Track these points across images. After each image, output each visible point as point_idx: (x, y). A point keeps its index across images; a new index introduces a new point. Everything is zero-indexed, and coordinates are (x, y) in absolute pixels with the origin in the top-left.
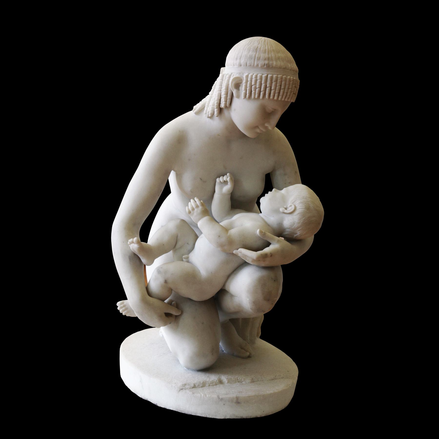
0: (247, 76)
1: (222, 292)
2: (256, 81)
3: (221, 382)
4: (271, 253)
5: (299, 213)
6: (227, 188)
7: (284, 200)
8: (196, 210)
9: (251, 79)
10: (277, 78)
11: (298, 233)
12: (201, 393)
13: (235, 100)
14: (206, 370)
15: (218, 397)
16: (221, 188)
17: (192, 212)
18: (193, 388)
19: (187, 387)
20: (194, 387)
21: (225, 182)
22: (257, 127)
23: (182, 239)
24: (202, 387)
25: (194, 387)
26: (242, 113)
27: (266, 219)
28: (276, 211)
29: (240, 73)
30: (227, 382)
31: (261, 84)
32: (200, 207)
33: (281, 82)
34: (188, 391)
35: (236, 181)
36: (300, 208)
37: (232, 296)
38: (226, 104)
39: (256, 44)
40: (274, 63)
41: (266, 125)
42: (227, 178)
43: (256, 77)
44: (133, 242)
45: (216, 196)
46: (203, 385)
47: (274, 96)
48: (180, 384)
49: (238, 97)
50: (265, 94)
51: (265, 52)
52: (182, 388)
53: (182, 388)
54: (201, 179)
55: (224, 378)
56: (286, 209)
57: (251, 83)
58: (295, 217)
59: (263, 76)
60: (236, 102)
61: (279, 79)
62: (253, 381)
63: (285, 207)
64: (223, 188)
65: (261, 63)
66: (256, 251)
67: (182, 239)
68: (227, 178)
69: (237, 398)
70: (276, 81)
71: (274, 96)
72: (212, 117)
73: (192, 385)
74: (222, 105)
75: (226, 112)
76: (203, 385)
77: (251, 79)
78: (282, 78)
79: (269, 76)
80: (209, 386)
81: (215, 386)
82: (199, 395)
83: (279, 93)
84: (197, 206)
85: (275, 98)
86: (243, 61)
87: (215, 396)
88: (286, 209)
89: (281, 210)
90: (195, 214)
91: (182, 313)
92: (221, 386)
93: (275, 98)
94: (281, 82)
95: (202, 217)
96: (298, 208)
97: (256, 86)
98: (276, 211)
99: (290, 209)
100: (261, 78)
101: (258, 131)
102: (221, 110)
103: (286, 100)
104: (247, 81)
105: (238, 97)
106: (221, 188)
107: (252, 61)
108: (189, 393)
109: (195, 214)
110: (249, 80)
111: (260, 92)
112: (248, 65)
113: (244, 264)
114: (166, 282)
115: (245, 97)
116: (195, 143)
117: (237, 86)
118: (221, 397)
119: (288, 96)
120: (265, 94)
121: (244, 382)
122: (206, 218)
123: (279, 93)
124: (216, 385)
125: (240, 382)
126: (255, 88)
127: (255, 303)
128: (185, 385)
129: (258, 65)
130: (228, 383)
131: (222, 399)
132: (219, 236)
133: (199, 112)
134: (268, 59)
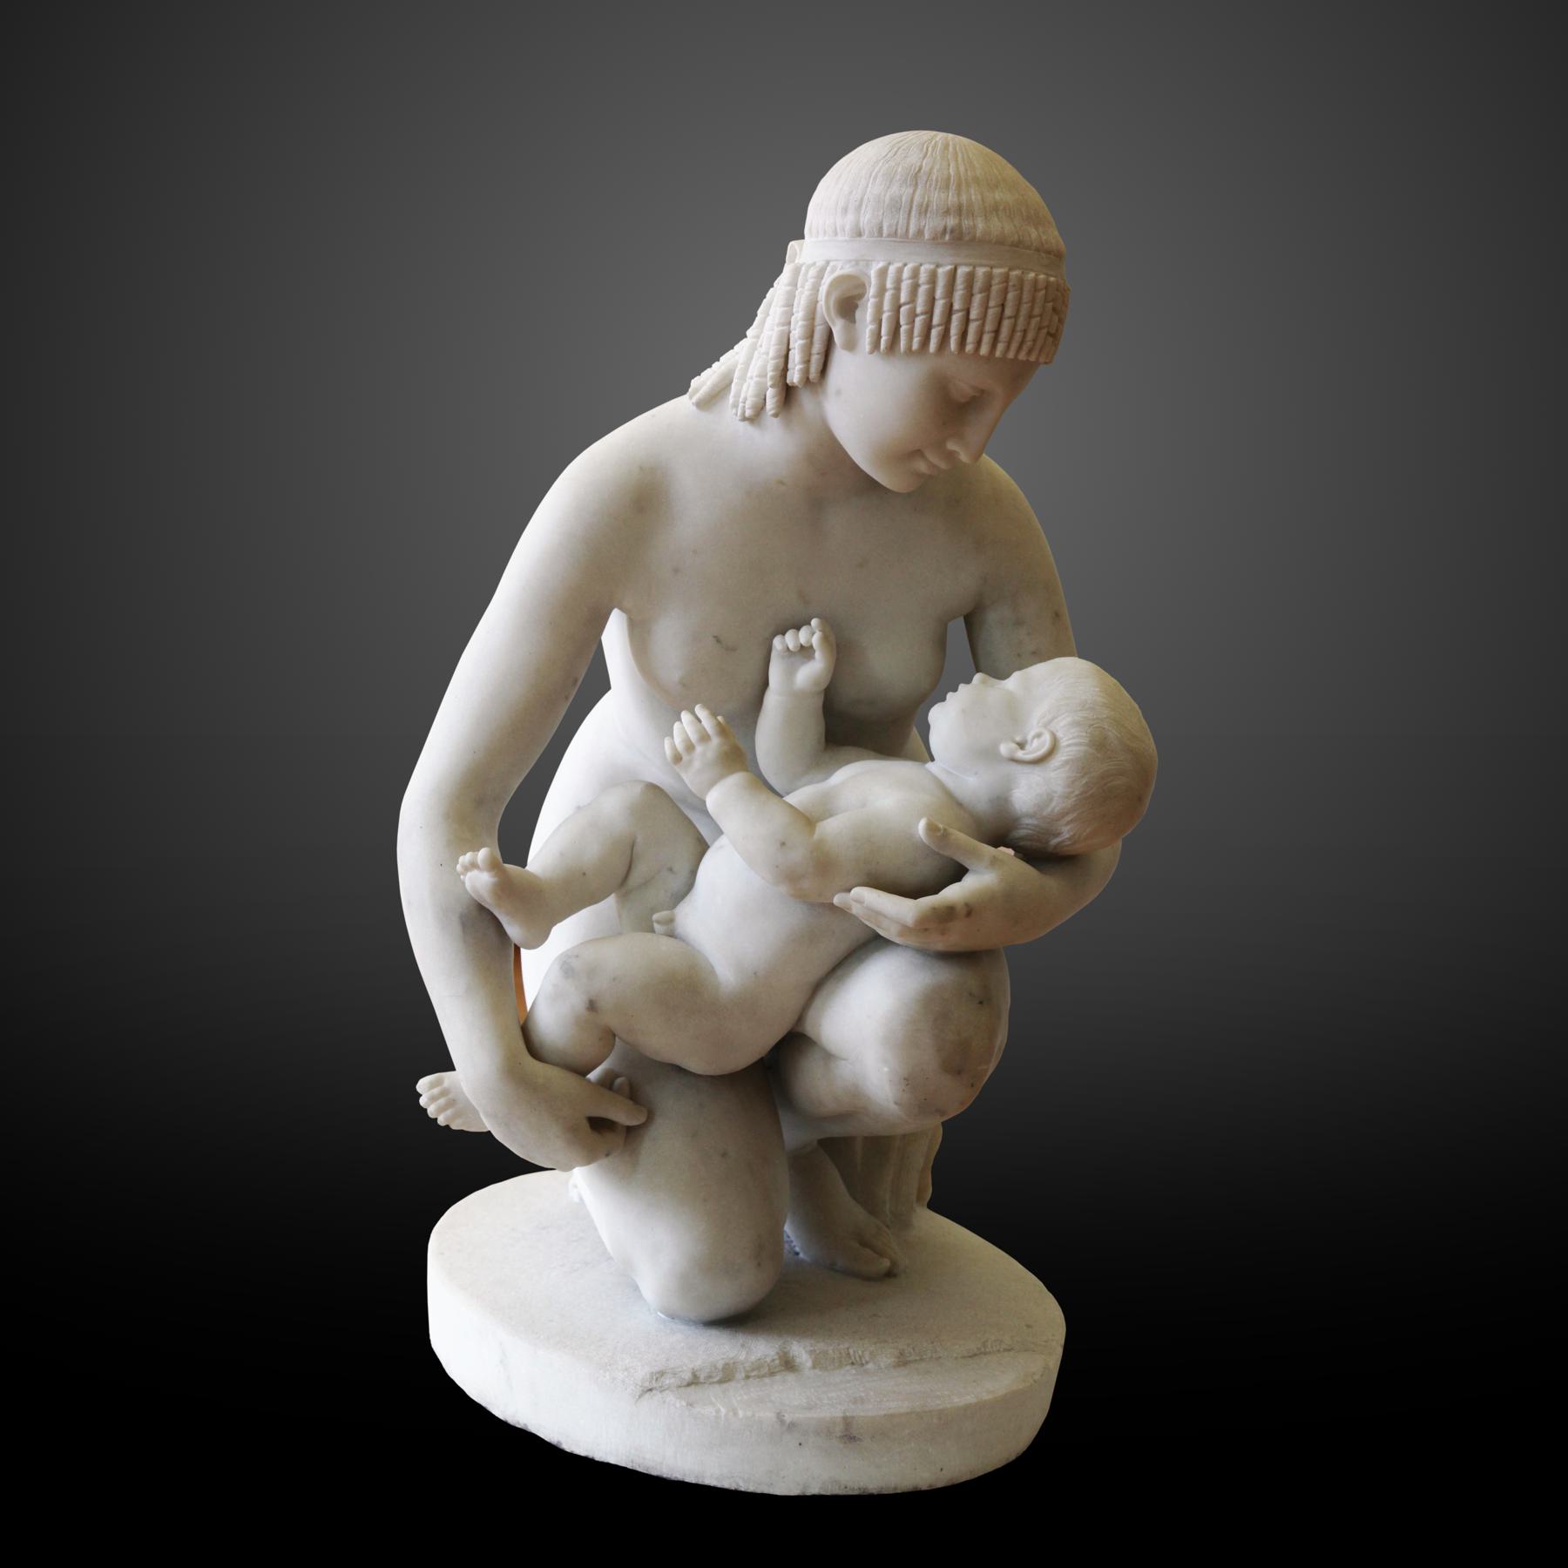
0: (883, 273)
1: (794, 1044)
2: (915, 288)
3: (788, 1365)
4: (967, 905)
5: (1067, 762)
6: (812, 672)
7: (1013, 713)
8: (699, 749)
9: (898, 281)
10: (989, 278)
11: (1066, 834)
12: (718, 1404)
13: (840, 358)
14: (736, 1321)
15: (780, 1417)
16: (790, 673)
17: (685, 758)
18: (689, 1385)
19: (668, 1381)
20: (694, 1381)
21: (805, 651)
22: (917, 453)
23: (647, 860)
24: (720, 1382)
25: (694, 1381)
26: (866, 402)
27: (950, 783)
28: (986, 754)
29: (857, 262)
30: (809, 1364)
31: (931, 301)
32: (716, 741)
33: (1005, 292)
34: (670, 1397)
35: (842, 648)
36: (1072, 745)
37: (829, 1057)
38: (806, 371)
39: (914, 158)
40: (980, 225)
41: (951, 446)
42: (811, 635)
43: (915, 274)
44: (474, 865)
45: (772, 699)
46: (726, 1375)
47: (979, 343)
48: (642, 1373)
49: (851, 345)
50: (945, 336)
51: (947, 187)
52: (652, 1386)
53: (652, 1386)
54: (718, 641)
55: (800, 1350)
56: (1021, 745)
57: (896, 297)
58: (1053, 774)
59: (940, 271)
60: (845, 366)
61: (995, 281)
62: (902, 1362)
63: (1018, 739)
64: (797, 673)
65: (931, 224)
66: (915, 898)
67: (647, 860)
68: (811, 635)
69: (848, 1422)
70: (987, 288)
71: (979, 343)
72: (756, 416)
73: (687, 1376)
74: (794, 377)
75: (806, 400)
76: (726, 1375)
77: (898, 281)
78: (1006, 279)
79: (962, 271)
80: (748, 1377)
81: (767, 1380)
82: (709, 1411)
83: (997, 332)
84: (704, 737)
85: (984, 350)
86: (866, 219)
87: (768, 1415)
88: (1021, 745)
89: (1005, 749)
90: (697, 764)
91: (650, 1117)
92: (790, 1377)
93: (984, 350)
94: (1005, 292)
95: (722, 777)
96: (1064, 742)
97: (914, 309)
98: (986, 754)
99: (1036, 748)
100: (933, 280)
101: (922, 467)
102: (788, 394)
103: (1022, 356)
104: (882, 290)
105: (851, 345)
106: (790, 673)
107: (902, 217)
108: (673, 1402)
109: (697, 764)
110: (889, 284)
111: (928, 327)
112: (885, 232)
113: (871, 943)
114: (592, 1006)
115: (876, 345)
116: (696, 512)
117: (848, 306)
118: (788, 1418)
119: (1029, 344)
120: (945, 336)
121: (870, 1366)
122: (735, 780)
123: (997, 332)
124: (772, 1374)
125: (857, 1363)
126: (913, 315)
127: (911, 1081)
128: (662, 1373)
129: (920, 233)
130: (814, 1367)
131: (792, 1426)
132: (783, 844)
133: (711, 401)
134: (959, 210)
